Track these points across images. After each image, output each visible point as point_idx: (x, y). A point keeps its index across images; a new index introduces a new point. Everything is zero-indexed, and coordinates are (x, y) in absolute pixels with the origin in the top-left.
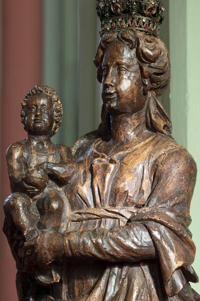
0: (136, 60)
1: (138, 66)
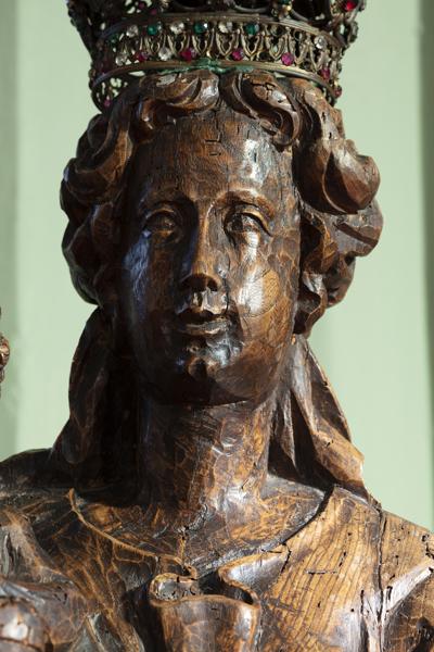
0: (291, 198)
1: (297, 217)
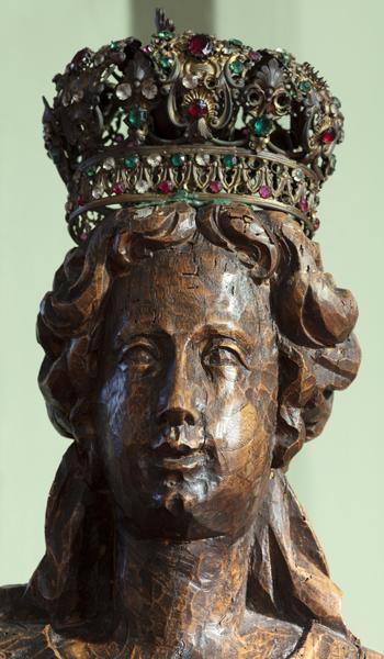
0: (268, 331)
1: (275, 351)
